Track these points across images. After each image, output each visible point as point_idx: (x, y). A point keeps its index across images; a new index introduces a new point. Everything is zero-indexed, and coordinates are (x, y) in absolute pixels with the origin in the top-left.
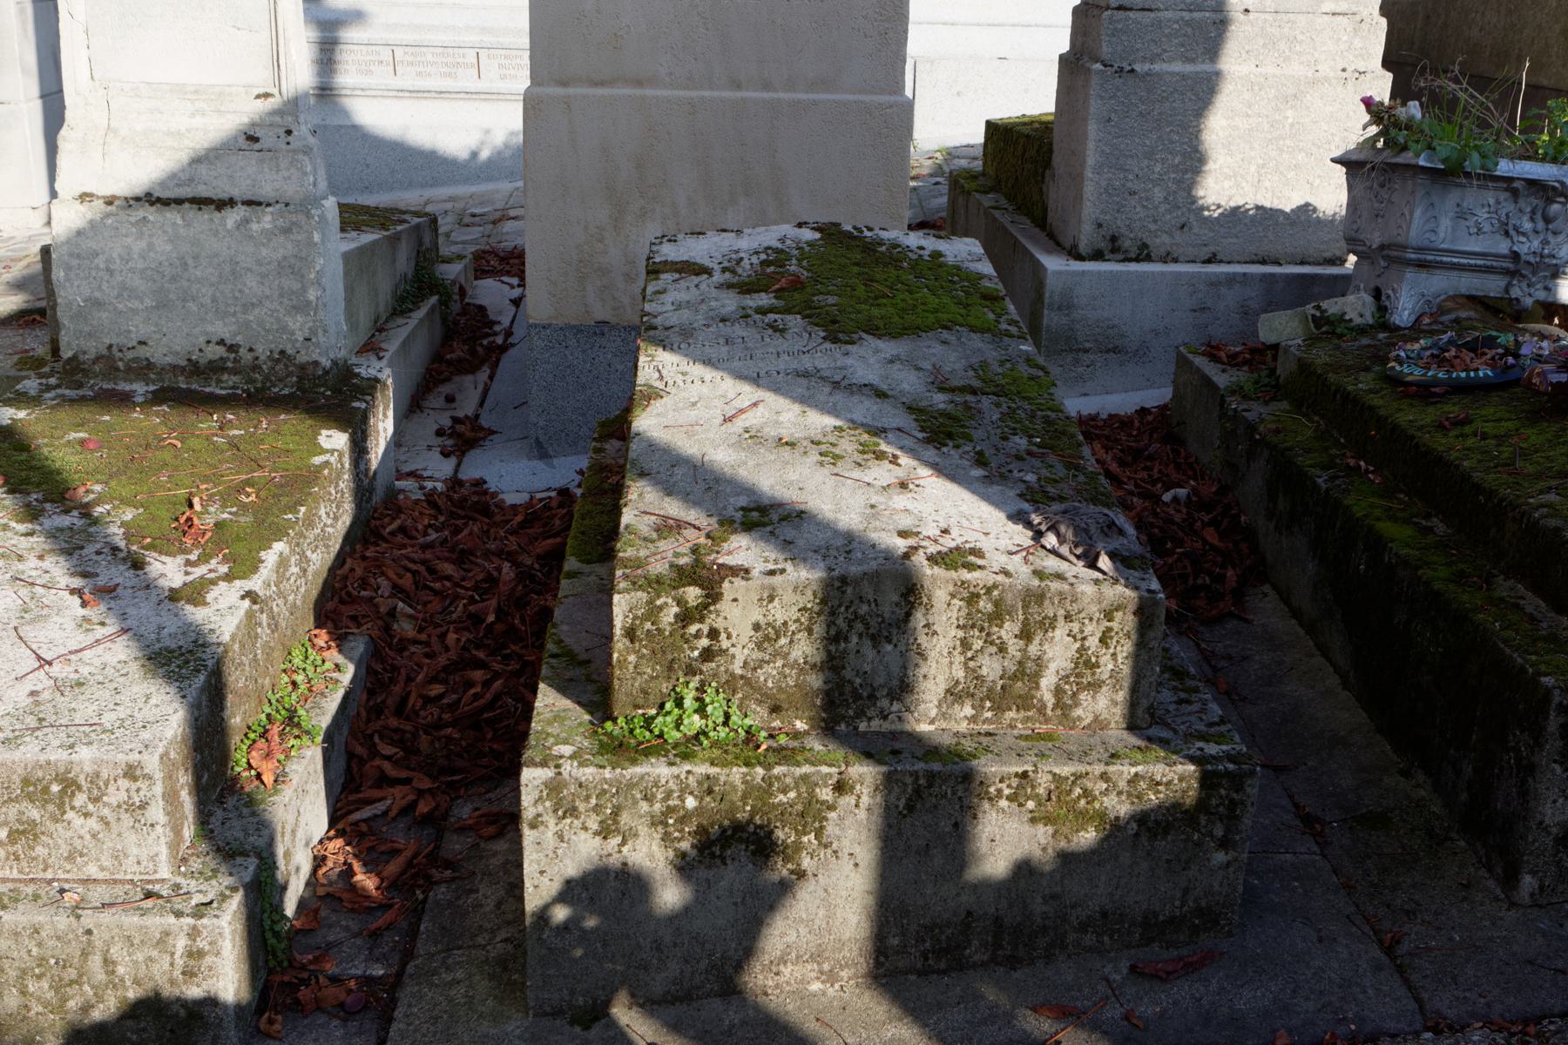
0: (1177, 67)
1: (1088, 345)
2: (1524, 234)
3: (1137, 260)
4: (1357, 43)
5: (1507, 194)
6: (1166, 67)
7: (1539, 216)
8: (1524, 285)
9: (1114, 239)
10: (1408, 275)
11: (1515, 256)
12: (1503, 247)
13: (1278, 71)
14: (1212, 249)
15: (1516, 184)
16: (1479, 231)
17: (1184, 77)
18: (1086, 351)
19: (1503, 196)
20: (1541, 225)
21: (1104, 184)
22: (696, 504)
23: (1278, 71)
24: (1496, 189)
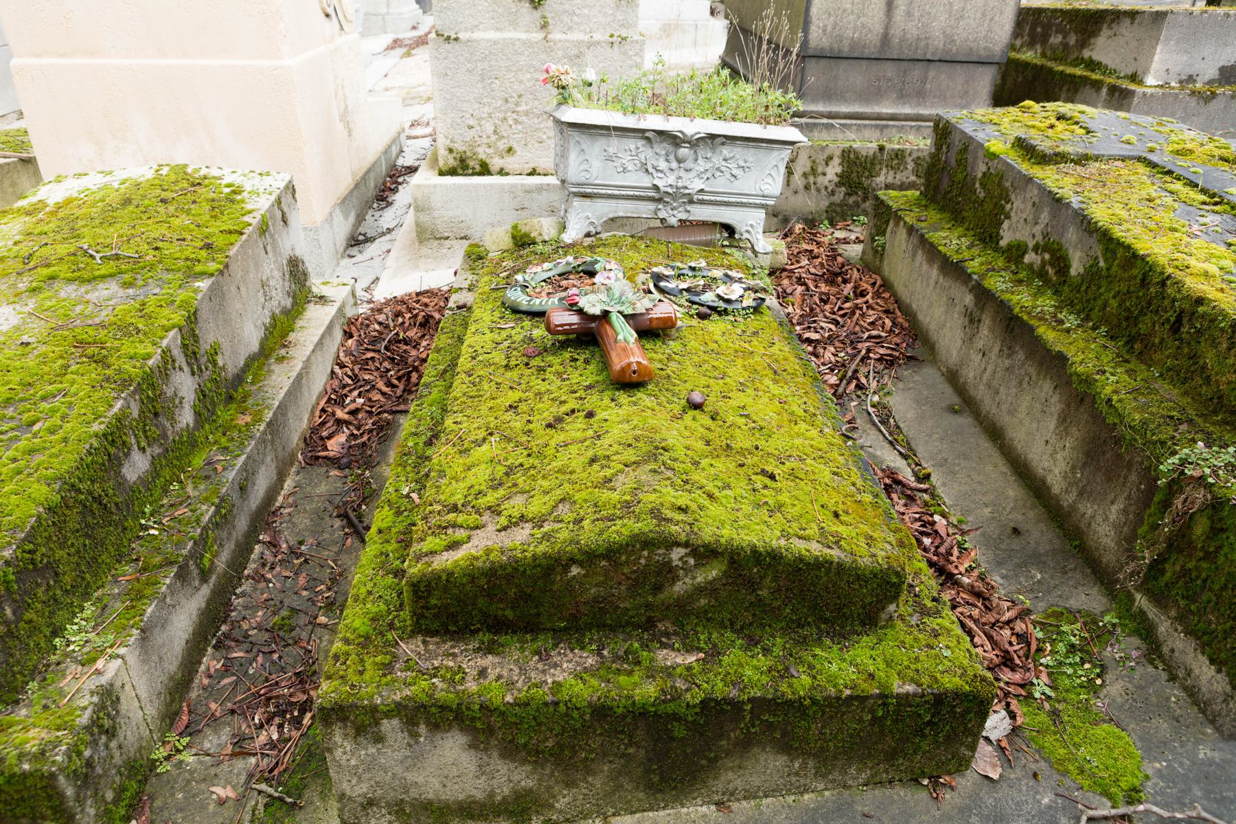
0: (492, 35)
1: (446, 235)
2: (661, 171)
3: (480, 174)
4: (620, 16)
5: (644, 142)
6: (523, 36)
7: (672, 157)
8: (668, 208)
9: (462, 161)
10: (575, 203)
11: (656, 188)
12: (646, 181)
13: (563, 37)
14: (532, 165)
15: (647, 134)
16: (625, 170)
17: (495, 43)
18: (447, 238)
19: (640, 143)
20: (674, 165)
21: (449, 121)
22: (1070, 75)
23: (563, 37)
24: (634, 137)
